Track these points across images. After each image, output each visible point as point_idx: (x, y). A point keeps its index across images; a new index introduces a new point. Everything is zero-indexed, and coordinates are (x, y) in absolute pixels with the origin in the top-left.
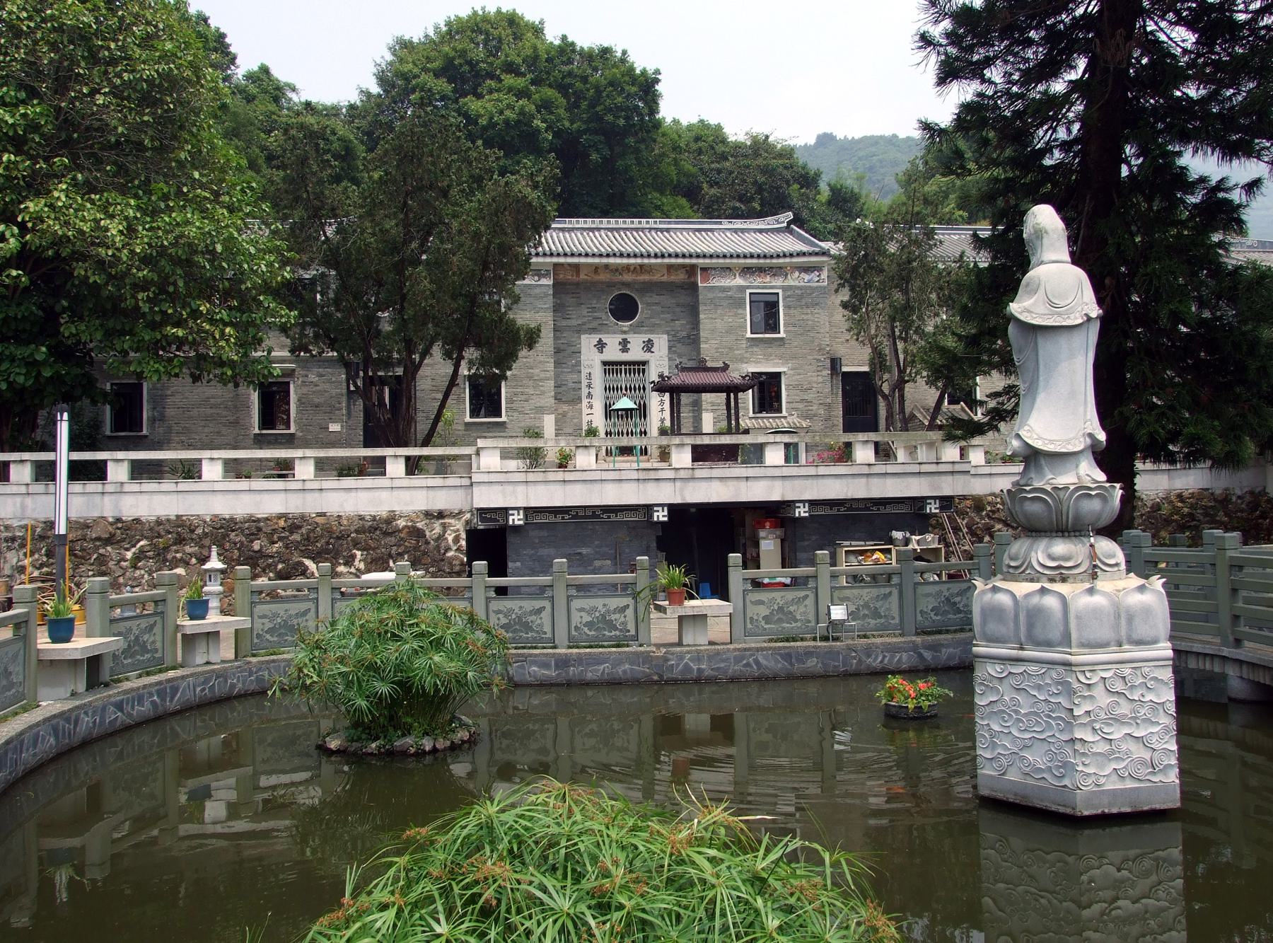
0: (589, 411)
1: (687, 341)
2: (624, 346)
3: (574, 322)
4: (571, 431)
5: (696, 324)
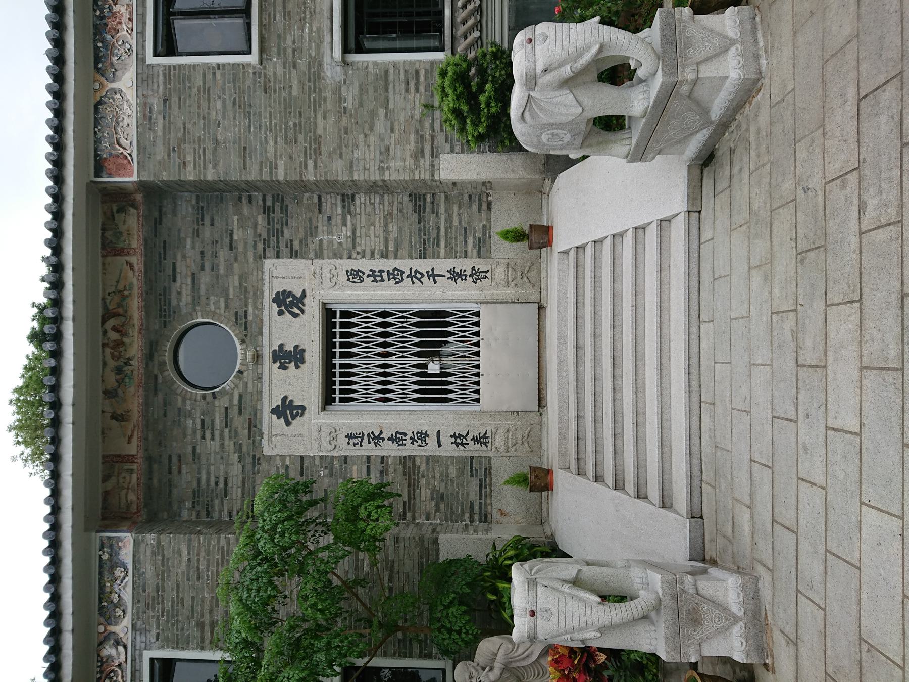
0: (432, 441)
1: (277, 215)
2: (288, 357)
3: (236, 470)
4: (474, 485)
5: (241, 192)
